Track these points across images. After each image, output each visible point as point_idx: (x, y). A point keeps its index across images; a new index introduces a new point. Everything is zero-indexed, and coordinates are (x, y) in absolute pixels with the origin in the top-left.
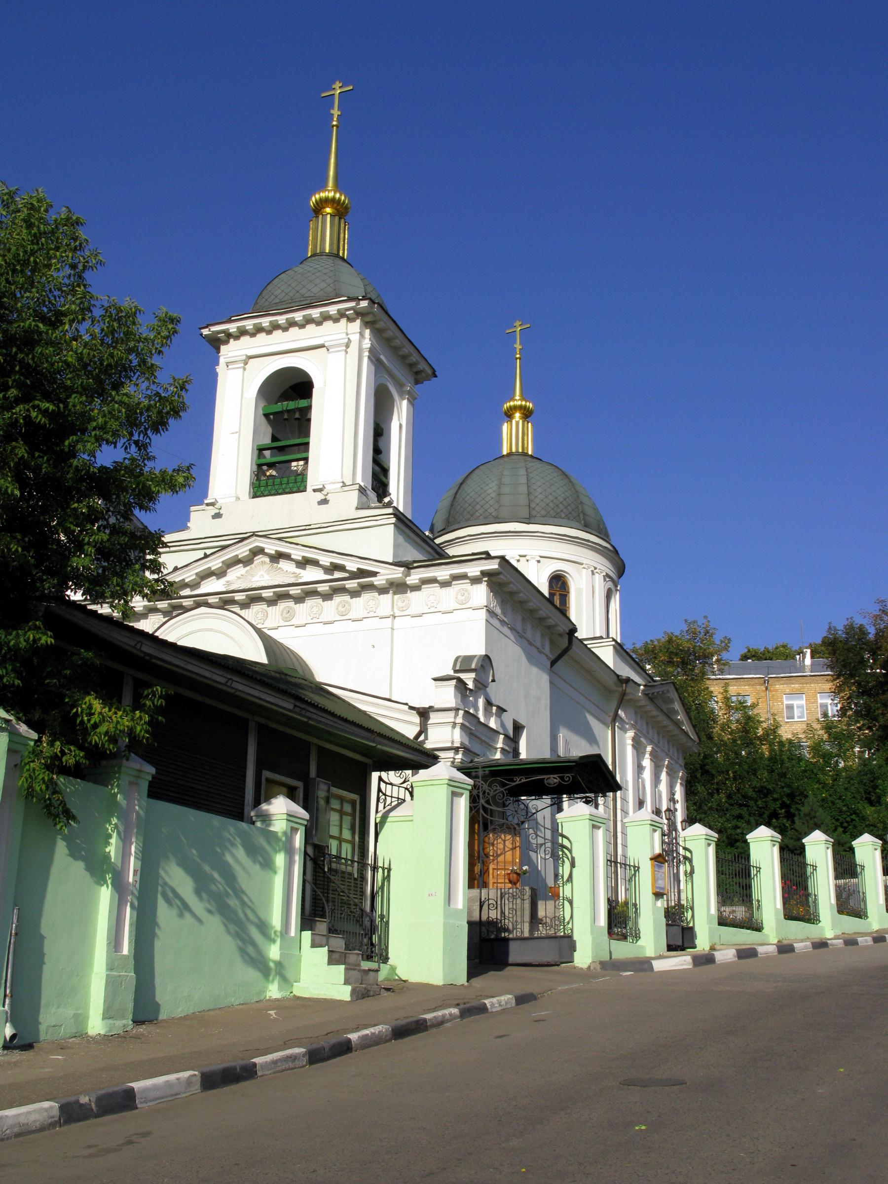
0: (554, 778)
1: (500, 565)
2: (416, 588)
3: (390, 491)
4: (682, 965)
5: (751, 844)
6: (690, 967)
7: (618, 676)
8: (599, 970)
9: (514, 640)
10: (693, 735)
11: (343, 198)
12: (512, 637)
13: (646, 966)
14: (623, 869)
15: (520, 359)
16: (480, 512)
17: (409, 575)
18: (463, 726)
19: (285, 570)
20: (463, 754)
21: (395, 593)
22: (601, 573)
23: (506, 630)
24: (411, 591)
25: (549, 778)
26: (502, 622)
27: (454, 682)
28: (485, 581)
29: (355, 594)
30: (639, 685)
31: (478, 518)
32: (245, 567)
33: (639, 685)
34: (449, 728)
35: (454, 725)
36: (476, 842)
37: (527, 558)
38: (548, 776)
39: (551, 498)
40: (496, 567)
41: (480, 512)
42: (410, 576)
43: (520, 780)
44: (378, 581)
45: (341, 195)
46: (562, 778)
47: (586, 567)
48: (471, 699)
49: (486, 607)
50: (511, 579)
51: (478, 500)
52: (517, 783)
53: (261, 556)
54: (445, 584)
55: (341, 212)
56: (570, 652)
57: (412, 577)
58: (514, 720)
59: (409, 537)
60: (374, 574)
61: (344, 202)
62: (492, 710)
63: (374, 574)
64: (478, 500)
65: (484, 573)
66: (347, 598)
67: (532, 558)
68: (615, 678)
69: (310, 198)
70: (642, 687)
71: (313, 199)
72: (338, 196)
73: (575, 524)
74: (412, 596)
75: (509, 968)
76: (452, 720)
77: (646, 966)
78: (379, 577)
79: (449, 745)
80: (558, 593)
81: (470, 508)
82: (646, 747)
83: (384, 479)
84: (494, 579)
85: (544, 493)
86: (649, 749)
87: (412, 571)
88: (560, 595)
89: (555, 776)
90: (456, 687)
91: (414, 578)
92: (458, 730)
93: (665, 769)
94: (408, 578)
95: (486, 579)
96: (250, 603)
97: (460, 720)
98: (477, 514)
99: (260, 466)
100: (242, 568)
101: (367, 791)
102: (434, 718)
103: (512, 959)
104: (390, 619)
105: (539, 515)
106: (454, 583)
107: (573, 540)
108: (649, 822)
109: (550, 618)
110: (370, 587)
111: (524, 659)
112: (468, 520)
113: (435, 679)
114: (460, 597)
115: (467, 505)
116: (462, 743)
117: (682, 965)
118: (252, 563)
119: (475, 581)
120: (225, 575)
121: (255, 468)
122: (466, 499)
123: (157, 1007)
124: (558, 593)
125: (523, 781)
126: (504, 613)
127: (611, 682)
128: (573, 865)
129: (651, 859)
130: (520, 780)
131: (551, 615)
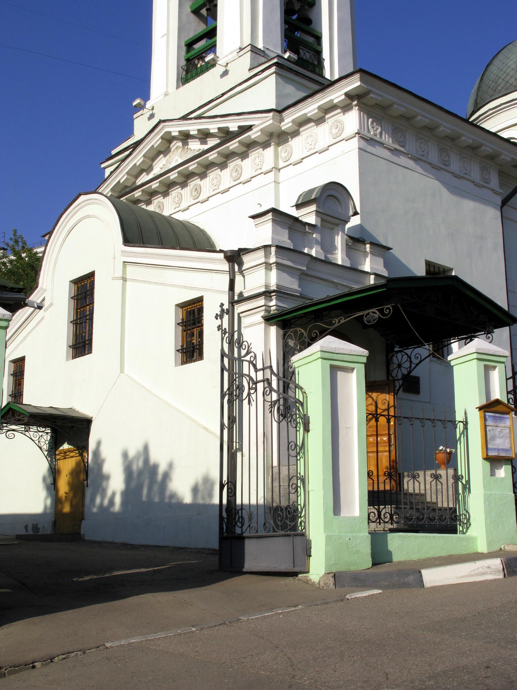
0: (374, 313)
1: (361, 80)
2: (295, 133)
3: (324, 58)
4: (483, 574)
6: (501, 576)
8: (332, 586)
9: (421, 171)
12: (419, 169)
13: (411, 579)
16: (502, 85)
17: (282, 120)
18: (278, 265)
19: (192, 149)
20: (276, 299)
21: (278, 144)
23: (403, 160)
24: (292, 138)
25: (368, 314)
26: (394, 151)
27: (270, 216)
28: (355, 105)
29: (244, 156)
31: (500, 92)
32: (165, 156)
34: (262, 271)
35: (268, 266)
38: (367, 312)
40: (358, 83)
41: (502, 85)
42: (283, 121)
43: (339, 322)
44: (254, 134)
46: (381, 311)
48: (314, 236)
49: (358, 133)
50: (395, 100)
51: (499, 75)
52: (336, 325)
53: (175, 142)
54: (319, 121)
57: (286, 121)
58: (426, 261)
59: (301, 84)
60: (249, 128)
62: (365, 249)
63: (249, 128)
64: (499, 75)
65: (348, 95)
66: (238, 162)
74: (295, 143)
76: (263, 260)
77: (411, 579)
78: (255, 130)
79: (263, 289)
81: (494, 84)
83: (318, 48)
84: (364, 100)
87: (284, 114)
89: (374, 310)
90: (274, 221)
91: (287, 124)
92: (274, 273)
94: (283, 124)
95: (355, 103)
96: (168, 190)
97: (273, 259)
98: (500, 88)
99: (188, 60)
100: (164, 158)
102: (248, 261)
103: (249, 565)
104: (272, 173)
106: (327, 117)
108: (475, 356)
109: (481, 145)
110: (251, 145)
111: (445, 193)
112: (492, 95)
113: (254, 217)
114: (335, 131)
115: (491, 82)
116: (278, 286)
117: (483, 574)
118: (170, 151)
119: (346, 108)
120: (152, 169)
121: (184, 63)
122: (490, 78)
123: (390, 554)
125: (342, 321)
126: (396, 140)
128: (307, 429)
129: (480, 408)
130: (339, 322)
131: (482, 141)
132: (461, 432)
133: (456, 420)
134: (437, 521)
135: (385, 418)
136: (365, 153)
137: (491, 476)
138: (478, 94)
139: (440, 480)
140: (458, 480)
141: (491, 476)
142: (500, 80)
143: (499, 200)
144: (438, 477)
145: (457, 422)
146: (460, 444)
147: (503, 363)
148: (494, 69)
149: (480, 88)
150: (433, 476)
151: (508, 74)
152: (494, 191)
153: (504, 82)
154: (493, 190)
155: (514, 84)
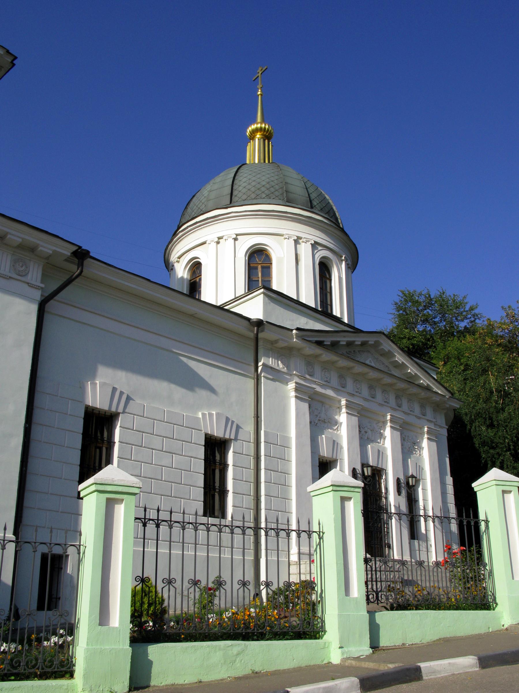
5: (478, 494)
7: (248, 319)
10: (439, 389)
11: (267, 127)
14: (272, 539)
15: (261, 95)
16: (195, 211)
22: (309, 241)
30: (292, 330)
33: (292, 330)
36: (217, 494)
37: (224, 238)
39: (254, 184)
45: (265, 125)
47: (287, 236)
55: (267, 136)
56: (83, 274)
61: (268, 130)
67: (229, 237)
68: (247, 322)
69: (246, 131)
70: (294, 331)
71: (248, 131)
72: (263, 126)
73: (281, 202)
75: (262, 591)
80: (260, 266)
82: (340, 401)
85: (247, 182)
86: (343, 402)
88: (263, 268)
93: (389, 424)
101: (111, 457)
105: (240, 200)
107: (268, 214)
124: (260, 266)
127: (242, 328)
132: (317, 544)
133: (480, 519)
134: (55, 666)
135: (216, 527)
136: (149, 283)
137: (101, 624)
138: (181, 220)
139: (406, 565)
140: (289, 587)
141: (101, 624)
142: (195, 207)
143: (38, 295)
144: (269, 585)
145: (481, 521)
146: (316, 555)
147: (134, 494)
148: (204, 200)
149: (184, 215)
150: (400, 563)
151: (201, 201)
152: (30, 285)
153: (197, 208)
154: (28, 283)
155: (203, 210)
